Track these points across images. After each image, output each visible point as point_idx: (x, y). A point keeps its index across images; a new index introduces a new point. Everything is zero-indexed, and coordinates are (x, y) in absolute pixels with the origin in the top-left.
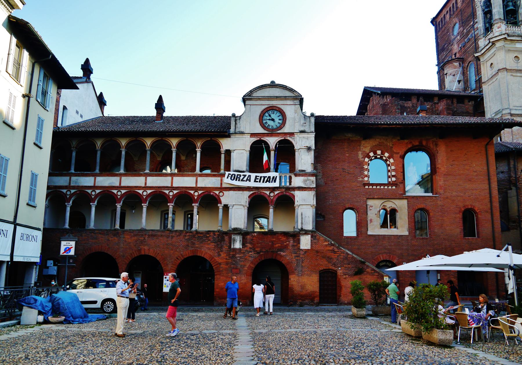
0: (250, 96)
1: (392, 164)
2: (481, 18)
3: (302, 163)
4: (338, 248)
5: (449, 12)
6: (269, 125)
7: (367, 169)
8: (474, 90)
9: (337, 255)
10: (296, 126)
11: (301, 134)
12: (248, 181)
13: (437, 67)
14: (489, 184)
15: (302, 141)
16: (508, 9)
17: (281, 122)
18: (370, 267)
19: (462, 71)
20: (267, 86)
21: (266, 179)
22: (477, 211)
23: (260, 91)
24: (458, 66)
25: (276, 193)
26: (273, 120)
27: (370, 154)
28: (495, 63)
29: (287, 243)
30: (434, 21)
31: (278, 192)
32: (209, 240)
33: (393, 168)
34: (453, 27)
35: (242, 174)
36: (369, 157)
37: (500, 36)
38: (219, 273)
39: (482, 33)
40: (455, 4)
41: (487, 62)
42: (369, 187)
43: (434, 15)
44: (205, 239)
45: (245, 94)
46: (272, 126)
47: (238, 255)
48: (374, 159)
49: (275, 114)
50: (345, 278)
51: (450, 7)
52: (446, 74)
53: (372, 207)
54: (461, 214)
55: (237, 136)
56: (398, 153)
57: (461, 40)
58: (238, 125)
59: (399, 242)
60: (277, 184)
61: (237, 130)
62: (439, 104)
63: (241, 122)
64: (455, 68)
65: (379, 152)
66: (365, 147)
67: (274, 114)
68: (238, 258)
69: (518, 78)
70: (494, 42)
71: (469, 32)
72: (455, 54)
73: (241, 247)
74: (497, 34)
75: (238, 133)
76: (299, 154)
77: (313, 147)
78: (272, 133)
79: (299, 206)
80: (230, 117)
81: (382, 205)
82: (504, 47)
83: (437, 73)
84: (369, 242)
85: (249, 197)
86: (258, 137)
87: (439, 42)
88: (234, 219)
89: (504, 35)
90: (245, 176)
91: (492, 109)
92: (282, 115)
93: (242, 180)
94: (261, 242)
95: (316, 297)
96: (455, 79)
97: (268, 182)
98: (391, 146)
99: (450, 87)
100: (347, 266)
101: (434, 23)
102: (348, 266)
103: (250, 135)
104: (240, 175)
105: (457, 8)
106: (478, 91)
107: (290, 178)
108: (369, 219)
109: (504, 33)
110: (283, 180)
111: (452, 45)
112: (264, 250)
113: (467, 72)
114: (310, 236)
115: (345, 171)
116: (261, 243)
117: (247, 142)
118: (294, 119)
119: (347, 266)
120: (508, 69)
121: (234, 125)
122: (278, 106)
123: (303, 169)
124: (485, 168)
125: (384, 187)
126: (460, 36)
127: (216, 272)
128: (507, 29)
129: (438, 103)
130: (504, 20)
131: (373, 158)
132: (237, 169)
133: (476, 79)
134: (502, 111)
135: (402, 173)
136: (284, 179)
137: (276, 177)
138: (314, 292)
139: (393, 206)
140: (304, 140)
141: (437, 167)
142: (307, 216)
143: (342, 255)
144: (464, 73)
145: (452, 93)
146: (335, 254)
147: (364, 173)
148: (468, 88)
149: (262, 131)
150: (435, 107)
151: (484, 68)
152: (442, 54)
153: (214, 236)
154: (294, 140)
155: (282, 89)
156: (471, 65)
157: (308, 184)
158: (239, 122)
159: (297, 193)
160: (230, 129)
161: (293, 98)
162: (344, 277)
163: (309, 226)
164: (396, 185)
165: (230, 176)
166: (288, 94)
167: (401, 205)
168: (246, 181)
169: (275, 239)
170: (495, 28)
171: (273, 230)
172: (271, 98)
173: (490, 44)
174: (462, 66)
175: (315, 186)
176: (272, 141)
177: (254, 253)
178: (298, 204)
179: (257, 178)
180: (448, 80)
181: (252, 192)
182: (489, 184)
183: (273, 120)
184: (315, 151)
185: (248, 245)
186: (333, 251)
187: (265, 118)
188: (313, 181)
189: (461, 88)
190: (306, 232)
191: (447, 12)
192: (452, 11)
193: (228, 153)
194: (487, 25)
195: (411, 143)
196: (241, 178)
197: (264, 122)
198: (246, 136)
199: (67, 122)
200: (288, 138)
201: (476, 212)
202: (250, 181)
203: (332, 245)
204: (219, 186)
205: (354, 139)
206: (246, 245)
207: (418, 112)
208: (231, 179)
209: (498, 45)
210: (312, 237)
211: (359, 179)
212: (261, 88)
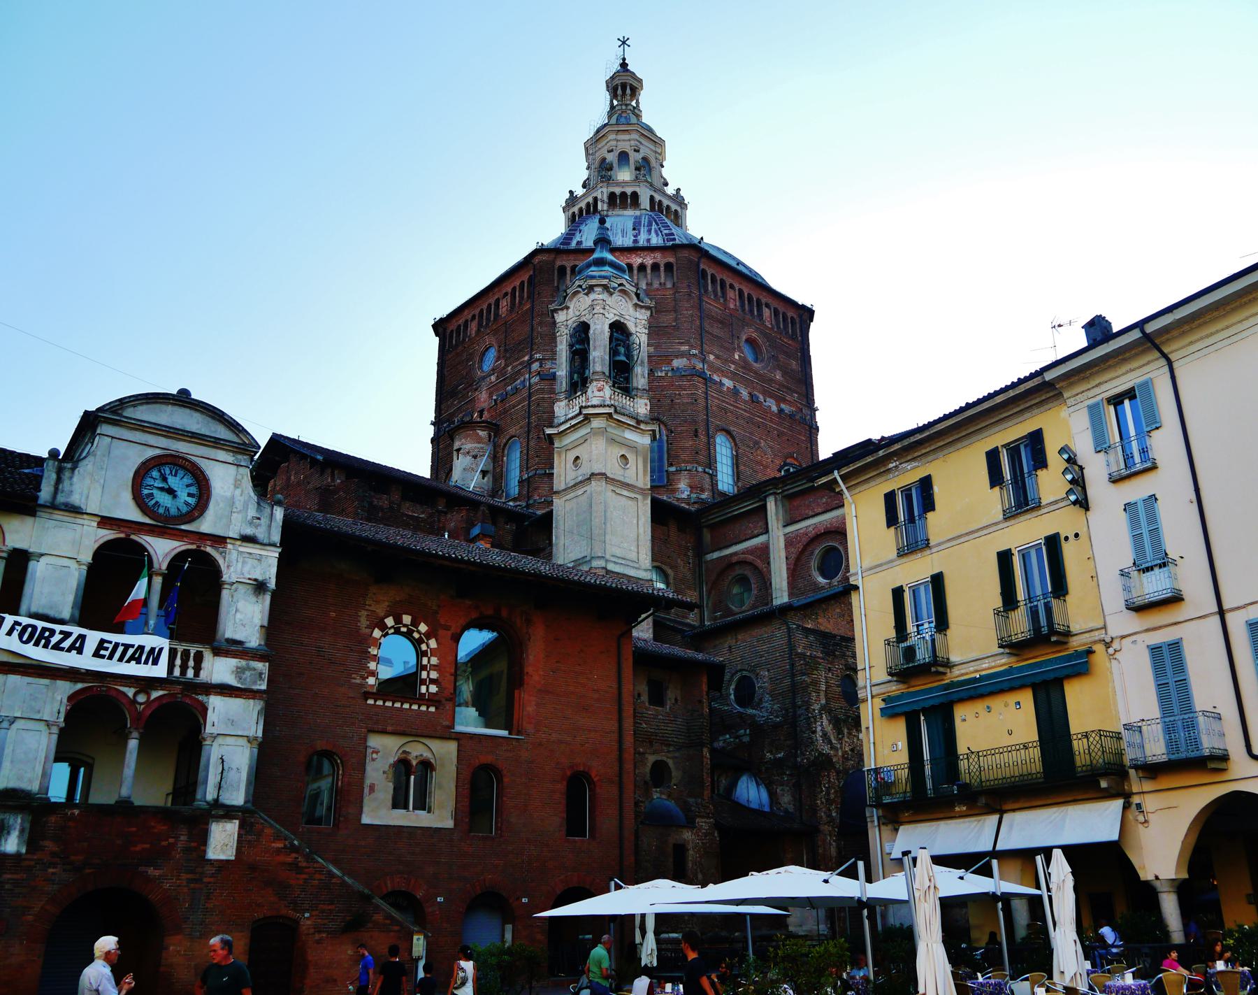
0: (115, 412)
1: (434, 653)
2: (564, 358)
3: (237, 621)
4: (308, 858)
5: (477, 317)
6: (157, 502)
7: (376, 656)
8: (514, 500)
9: (304, 876)
10: (233, 521)
11: (244, 544)
12: (74, 652)
13: (432, 427)
14: (620, 720)
15: (244, 562)
16: (618, 358)
17: (192, 501)
18: (383, 909)
19: (492, 452)
20: (169, 399)
21: (131, 651)
22: (595, 779)
23: (144, 407)
24: (486, 440)
25: (155, 694)
26: (171, 492)
27: (386, 620)
28: (584, 457)
30: (440, 327)
31: (161, 693)
33: (434, 661)
34: (483, 354)
35: (58, 628)
36: (383, 627)
37: (601, 408)
39: (563, 390)
40: (493, 306)
41: (568, 452)
42: (375, 701)
45: (104, 406)
46: (167, 509)
47: (9, 876)
48: (392, 634)
49: (178, 478)
50: (318, 942)
51: (482, 310)
52: (458, 450)
53: (377, 753)
54: (565, 783)
55: (58, 515)
56: (447, 628)
57: (499, 385)
58: (66, 484)
60: (160, 671)
61: (61, 499)
62: (449, 516)
63: (75, 479)
64: (479, 443)
65: (407, 619)
66: (378, 602)
67: (176, 475)
68: (7, 886)
69: (624, 499)
70: (589, 416)
72: (481, 413)
73: (24, 850)
74: (595, 401)
75: (63, 507)
76: (232, 596)
77: (272, 584)
78: (165, 526)
79: (215, 737)
80: (39, 461)
81: (401, 751)
82: (606, 431)
83: (432, 442)
85: (70, 698)
86: (122, 529)
87: (446, 373)
88: (12, 762)
89: (610, 407)
90: (67, 635)
91: (569, 551)
92: (198, 483)
93: (57, 647)
96: (477, 465)
97: (133, 662)
98: (435, 608)
99: (463, 480)
100: (326, 907)
101: (441, 330)
102: (330, 907)
103: (98, 519)
104: (53, 632)
105: (497, 315)
106: (524, 504)
107: (199, 658)
108: (368, 782)
109: (608, 402)
110: (178, 662)
111: (476, 390)
113: (503, 456)
117: (89, 538)
118: (231, 502)
119: (326, 907)
120: (609, 478)
121: (53, 483)
123: (238, 637)
124: (615, 685)
125: (410, 706)
126: (498, 378)
128: (612, 397)
129: (446, 513)
130: (610, 377)
131: (392, 631)
132: (41, 611)
133: (521, 477)
134: (590, 561)
135: (453, 677)
136: (182, 659)
137: (161, 650)
139: (425, 755)
140: (250, 562)
141: (525, 671)
142: (234, 768)
143: (317, 876)
144: (496, 458)
145: (464, 493)
146: (298, 876)
147: (369, 665)
148: (500, 492)
149: (134, 514)
150: (439, 521)
151: (560, 463)
154: (225, 558)
155: (210, 416)
156: (513, 442)
157: (248, 680)
158: (71, 478)
159: (216, 704)
160: (40, 491)
161: (233, 447)
162: (317, 937)
163: (237, 797)
164: (437, 704)
165: (19, 628)
166: (222, 432)
167: (444, 752)
168: (69, 650)
169: (134, 829)
170: (592, 388)
171: (133, 803)
172: (171, 432)
173: (581, 418)
174: (493, 441)
175: (264, 687)
176: (162, 549)
177: (64, 870)
178: (215, 731)
179: (106, 645)
180: (460, 464)
181: (80, 686)
182: (620, 720)
183: (171, 492)
184: (275, 595)
185: (47, 843)
186: (295, 867)
187: (149, 481)
188: (261, 674)
189: (486, 488)
190: (227, 812)
191: (474, 317)
192: (484, 318)
194: (576, 376)
196: (54, 640)
197: (146, 492)
198: (86, 522)
199: (635, 564)
200: (209, 549)
201: (591, 782)
202: (80, 651)
203: (294, 849)
206: (41, 842)
207: (475, 537)
208: (21, 636)
209: (596, 423)
210: (241, 827)
211: (355, 679)
212: (150, 399)
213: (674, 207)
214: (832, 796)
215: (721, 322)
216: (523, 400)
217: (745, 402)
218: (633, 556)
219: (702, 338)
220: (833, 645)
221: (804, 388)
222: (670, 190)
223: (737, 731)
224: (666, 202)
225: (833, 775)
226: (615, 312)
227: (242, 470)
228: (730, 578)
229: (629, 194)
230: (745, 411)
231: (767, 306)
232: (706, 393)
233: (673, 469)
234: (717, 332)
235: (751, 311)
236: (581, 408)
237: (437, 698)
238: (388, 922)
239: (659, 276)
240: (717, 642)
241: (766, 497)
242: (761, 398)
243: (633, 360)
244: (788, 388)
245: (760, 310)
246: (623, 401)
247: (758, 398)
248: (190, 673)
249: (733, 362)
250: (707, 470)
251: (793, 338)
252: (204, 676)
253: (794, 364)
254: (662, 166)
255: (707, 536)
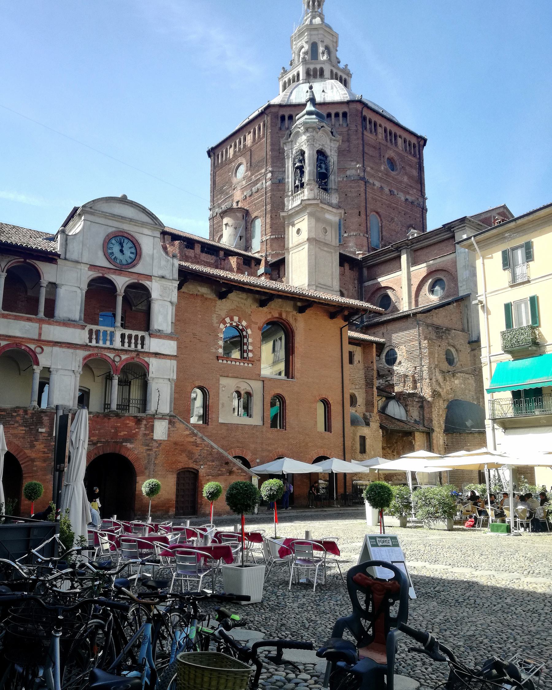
6: (116, 257)
29: (137, 430)
32: (17, 422)
38: (31, 475)
43: (214, 145)
44: (10, 419)
52: (226, 225)
53: (224, 387)
56: (256, 323)
59: (253, 433)
71: (258, 181)
72: (237, 202)
78: (121, 269)
84: (219, 432)
85: (84, 359)
94: (99, 427)
95: (171, 507)
98: (249, 313)
100: (211, 463)
103: (88, 266)
108: (221, 402)
111: (234, 189)
112: (103, 440)
114: (167, 421)
115: (196, 336)
116: (99, 429)
119: (211, 463)
122: (132, 233)
123: (160, 328)
127: (25, 474)
138: (169, 500)
146: (197, 448)
149: (106, 264)
150: (221, 264)
152: (219, 197)
153: (26, 416)
162: (207, 478)
169: (119, 425)
193: (53, 286)
195: (270, 313)
204: (36, 337)
205: (209, 297)
213: (344, 76)
214: (441, 413)
215: (374, 147)
216: (262, 196)
217: (387, 195)
218: (329, 284)
219: (363, 157)
220: (442, 333)
221: (420, 186)
222: (341, 66)
223: (387, 378)
224: (340, 73)
225: (441, 402)
226: (319, 143)
227: (156, 239)
228: (379, 295)
229: (312, 69)
230: (387, 200)
231: (400, 137)
232: (366, 190)
233: (345, 235)
234: (371, 153)
235: (391, 140)
236: (302, 200)
237: (252, 360)
238: (240, 471)
239: (339, 120)
240: (376, 331)
241: (401, 251)
242: (396, 192)
243: (329, 172)
244: (411, 187)
245: (395, 139)
246: (325, 196)
247: (394, 192)
248: (139, 346)
249: (381, 172)
250: (365, 235)
251: (414, 156)
252: (146, 349)
253: (415, 173)
254: (337, 51)
255: (365, 272)
